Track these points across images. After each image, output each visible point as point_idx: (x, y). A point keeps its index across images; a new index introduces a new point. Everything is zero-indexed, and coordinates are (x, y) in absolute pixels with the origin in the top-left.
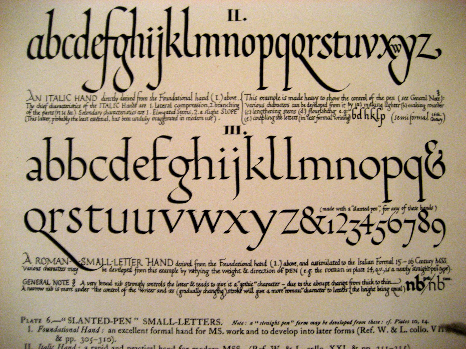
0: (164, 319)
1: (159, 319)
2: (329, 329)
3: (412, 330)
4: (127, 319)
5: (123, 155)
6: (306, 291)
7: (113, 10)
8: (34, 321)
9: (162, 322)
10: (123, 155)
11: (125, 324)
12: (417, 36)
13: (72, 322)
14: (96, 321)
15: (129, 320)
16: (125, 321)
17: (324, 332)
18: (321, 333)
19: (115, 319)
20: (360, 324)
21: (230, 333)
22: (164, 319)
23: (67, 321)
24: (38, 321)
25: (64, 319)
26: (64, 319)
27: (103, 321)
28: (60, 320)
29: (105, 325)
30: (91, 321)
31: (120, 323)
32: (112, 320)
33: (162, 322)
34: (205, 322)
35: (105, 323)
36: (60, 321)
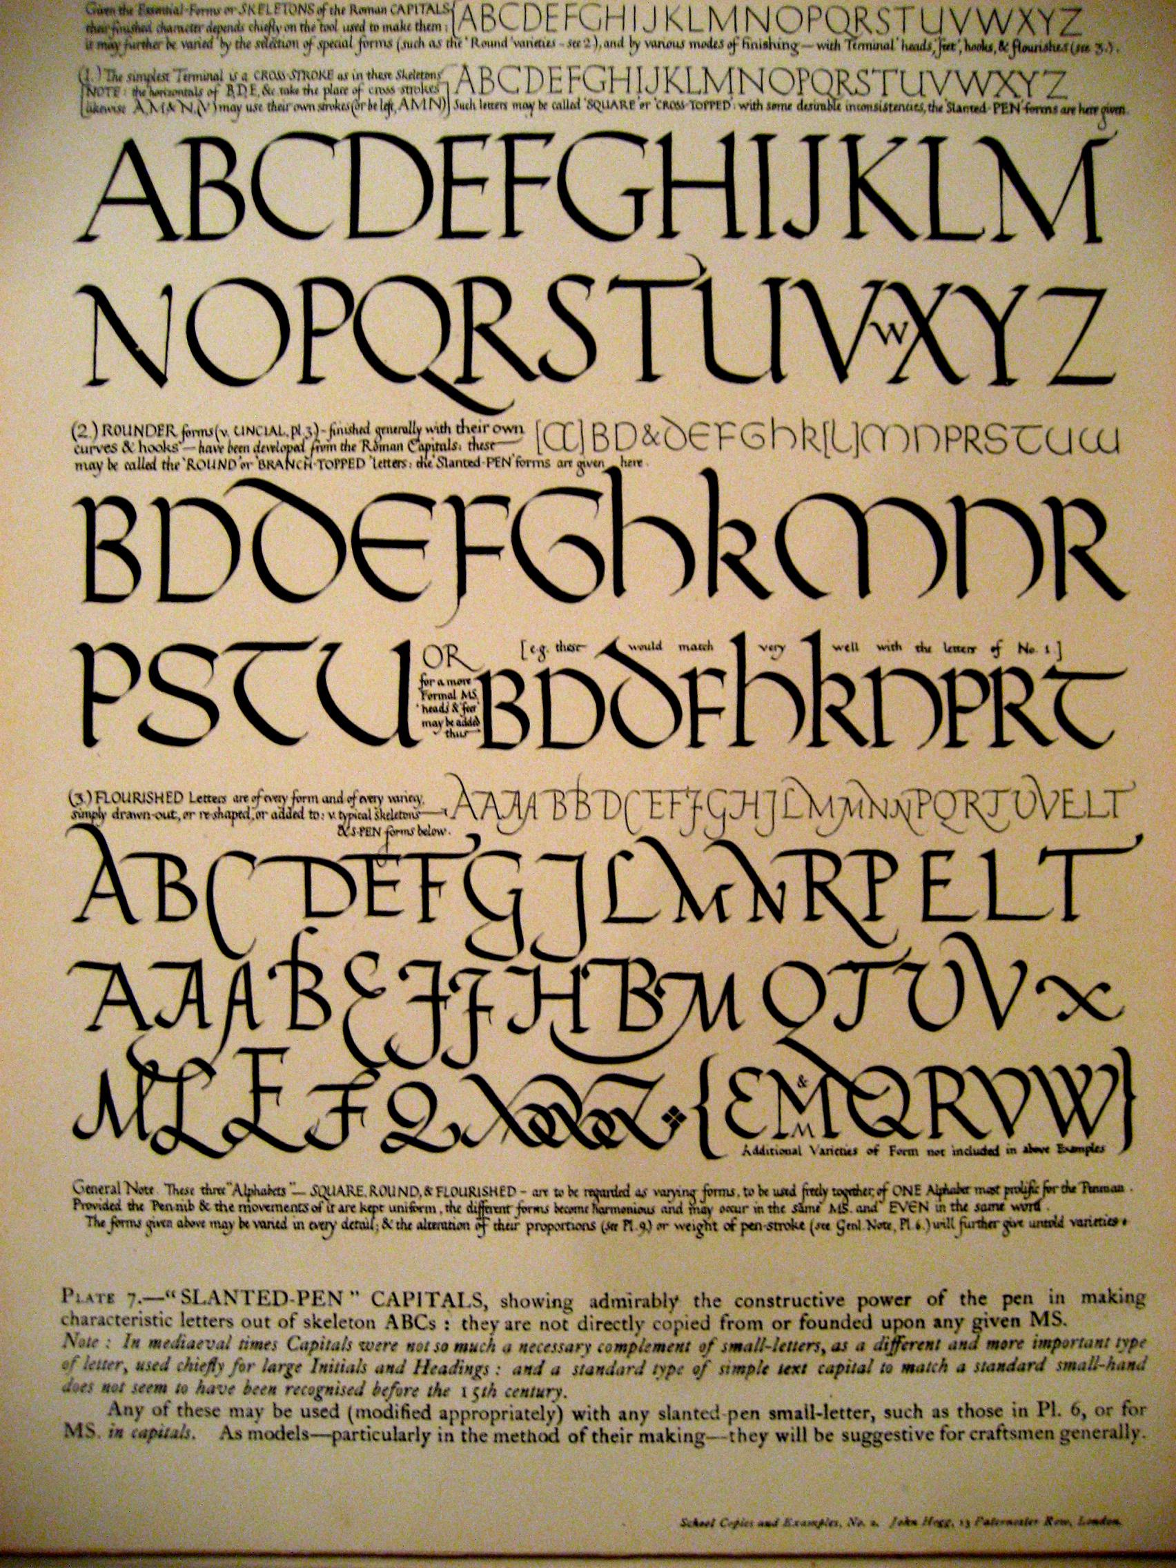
0: (461, 1294)
1: (394, 1294)
2: (904, 1295)
3: (740, 1303)
4: (331, 1294)
5: (97, 707)
6: (772, 1226)
7: (653, 1022)
8: (96, 1299)
9: (456, 1301)
10: (97, 707)
11: (327, 1306)
12: (1064, 501)
13: (193, 1300)
14: (254, 1299)
15: (337, 1296)
16: (326, 1297)
17: (529, 1415)
18: (521, 1418)
19: (300, 1293)
20: (296, 1363)
21: (889, 1303)
22: (461, 1294)
23: (179, 1297)
24: (105, 1299)
25: (170, 1294)
26: (170, 1294)
27: (271, 1298)
28: (163, 1295)
29: (276, 1308)
30: (241, 1298)
31: (315, 1304)
32: (293, 1295)
33: (456, 1302)
34: (260, 1298)
35: (276, 1304)
36: (162, 1299)
